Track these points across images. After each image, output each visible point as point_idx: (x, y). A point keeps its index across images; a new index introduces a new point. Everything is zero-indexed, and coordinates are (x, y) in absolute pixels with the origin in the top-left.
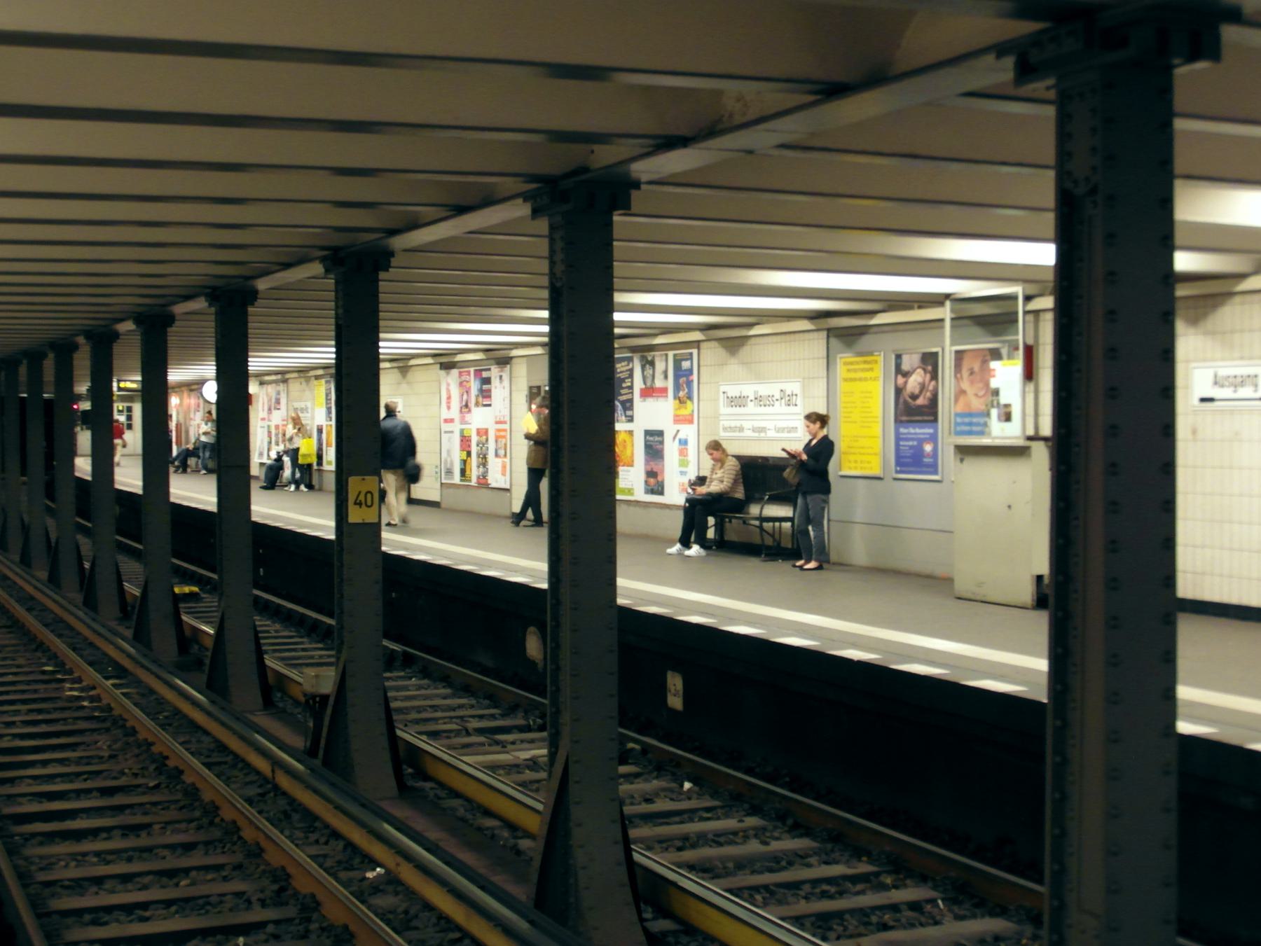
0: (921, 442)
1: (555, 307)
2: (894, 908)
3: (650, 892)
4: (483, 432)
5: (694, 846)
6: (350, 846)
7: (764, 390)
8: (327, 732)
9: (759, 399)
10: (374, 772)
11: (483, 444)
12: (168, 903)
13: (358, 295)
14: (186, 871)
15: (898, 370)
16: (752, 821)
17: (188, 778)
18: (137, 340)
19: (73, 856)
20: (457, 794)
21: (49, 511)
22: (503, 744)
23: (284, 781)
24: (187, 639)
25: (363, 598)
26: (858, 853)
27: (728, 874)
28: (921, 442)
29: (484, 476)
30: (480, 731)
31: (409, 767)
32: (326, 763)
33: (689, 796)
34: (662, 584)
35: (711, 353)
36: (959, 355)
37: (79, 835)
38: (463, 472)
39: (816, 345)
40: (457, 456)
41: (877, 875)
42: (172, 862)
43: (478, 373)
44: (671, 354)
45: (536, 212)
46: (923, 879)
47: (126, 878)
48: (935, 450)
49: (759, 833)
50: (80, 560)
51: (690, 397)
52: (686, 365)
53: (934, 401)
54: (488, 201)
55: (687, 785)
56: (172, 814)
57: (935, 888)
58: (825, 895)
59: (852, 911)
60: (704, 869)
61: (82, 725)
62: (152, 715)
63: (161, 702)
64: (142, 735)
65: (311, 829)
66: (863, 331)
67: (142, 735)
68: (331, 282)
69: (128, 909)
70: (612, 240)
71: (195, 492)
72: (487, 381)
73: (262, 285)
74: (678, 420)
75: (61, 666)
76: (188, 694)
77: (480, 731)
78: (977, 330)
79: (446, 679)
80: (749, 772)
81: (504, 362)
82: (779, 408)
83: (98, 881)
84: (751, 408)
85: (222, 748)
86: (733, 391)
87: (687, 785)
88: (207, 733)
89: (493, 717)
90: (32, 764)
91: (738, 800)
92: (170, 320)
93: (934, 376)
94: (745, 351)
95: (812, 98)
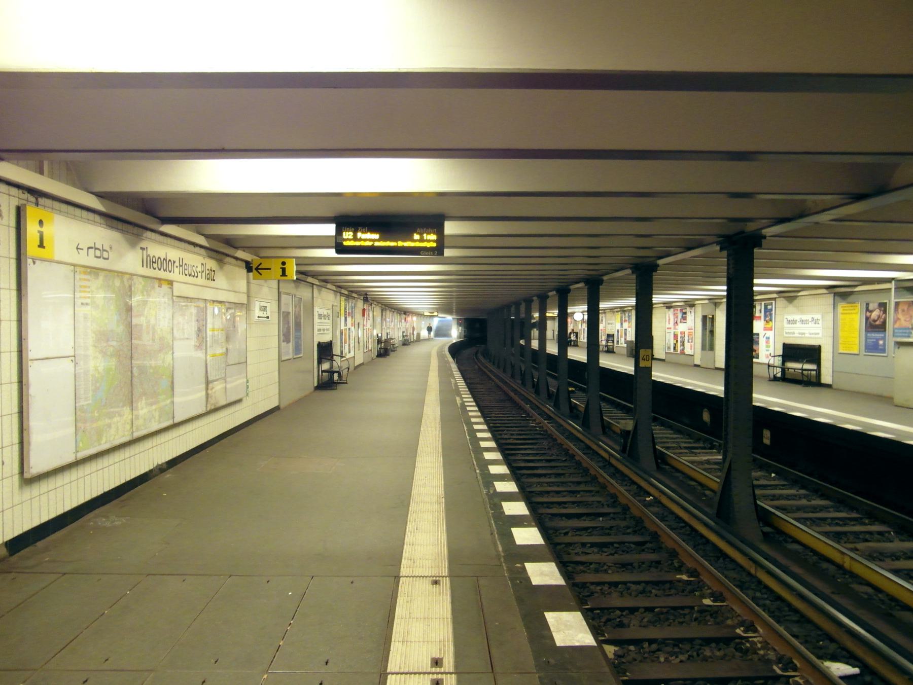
0: (878, 340)
1: (729, 284)
2: (870, 533)
3: (764, 517)
4: (683, 333)
5: (778, 499)
6: (639, 487)
7: (804, 317)
8: (629, 444)
9: (802, 321)
10: (648, 461)
11: (683, 338)
12: (573, 503)
13: (644, 280)
14: (579, 492)
15: (867, 310)
16: (803, 492)
17: (577, 458)
18: (557, 298)
19: (539, 483)
20: (678, 471)
21: (522, 361)
22: (696, 453)
23: (613, 461)
24: (573, 407)
25: (644, 396)
26: (852, 509)
27: (794, 512)
28: (878, 340)
29: (683, 350)
30: (686, 448)
31: (661, 459)
32: (629, 456)
33: (774, 479)
34: (765, 397)
35: (781, 303)
36: (897, 304)
37: (540, 476)
38: (675, 348)
39: (830, 299)
40: (672, 342)
41: (861, 518)
42: (574, 488)
43: (681, 310)
44: (763, 303)
45: (721, 249)
46: (883, 522)
47: (558, 492)
48: (884, 344)
49: (805, 496)
50: (533, 378)
51: (771, 320)
52: (769, 307)
53: (884, 323)
54: (700, 245)
55: (773, 475)
56: (572, 471)
57: (889, 526)
58: (837, 524)
59: (851, 533)
60: (782, 509)
61: (538, 436)
62: (563, 434)
63: (565, 430)
64: (559, 441)
65: (623, 480)
66: (852, 293)
67: (559, 441)
68: (634, 276)
69: (560, 503)
70: (753, 259)
71: (578, 355)
72: (685, 313)
73: (605, 278)
74: (765, 329)
75: (528, 415)
76: (575, 426)
77: (686, 448)
78: (905, 292)
79: (670, 427)
80: (799, 471)
81: (692, 305)
82: (811, 325)
83: (548, 492)
84: (798, 325)
85: (589, 448)
86: (790, 318)
87: (773, 475)
88: (582, 441)
89: (690, 443)
90: (521, 449)
91: (796, 482)
92: (569, 291)
93: (885, 312)
94: (796, 302)
95: (847, 201)
